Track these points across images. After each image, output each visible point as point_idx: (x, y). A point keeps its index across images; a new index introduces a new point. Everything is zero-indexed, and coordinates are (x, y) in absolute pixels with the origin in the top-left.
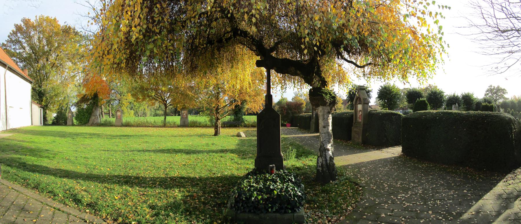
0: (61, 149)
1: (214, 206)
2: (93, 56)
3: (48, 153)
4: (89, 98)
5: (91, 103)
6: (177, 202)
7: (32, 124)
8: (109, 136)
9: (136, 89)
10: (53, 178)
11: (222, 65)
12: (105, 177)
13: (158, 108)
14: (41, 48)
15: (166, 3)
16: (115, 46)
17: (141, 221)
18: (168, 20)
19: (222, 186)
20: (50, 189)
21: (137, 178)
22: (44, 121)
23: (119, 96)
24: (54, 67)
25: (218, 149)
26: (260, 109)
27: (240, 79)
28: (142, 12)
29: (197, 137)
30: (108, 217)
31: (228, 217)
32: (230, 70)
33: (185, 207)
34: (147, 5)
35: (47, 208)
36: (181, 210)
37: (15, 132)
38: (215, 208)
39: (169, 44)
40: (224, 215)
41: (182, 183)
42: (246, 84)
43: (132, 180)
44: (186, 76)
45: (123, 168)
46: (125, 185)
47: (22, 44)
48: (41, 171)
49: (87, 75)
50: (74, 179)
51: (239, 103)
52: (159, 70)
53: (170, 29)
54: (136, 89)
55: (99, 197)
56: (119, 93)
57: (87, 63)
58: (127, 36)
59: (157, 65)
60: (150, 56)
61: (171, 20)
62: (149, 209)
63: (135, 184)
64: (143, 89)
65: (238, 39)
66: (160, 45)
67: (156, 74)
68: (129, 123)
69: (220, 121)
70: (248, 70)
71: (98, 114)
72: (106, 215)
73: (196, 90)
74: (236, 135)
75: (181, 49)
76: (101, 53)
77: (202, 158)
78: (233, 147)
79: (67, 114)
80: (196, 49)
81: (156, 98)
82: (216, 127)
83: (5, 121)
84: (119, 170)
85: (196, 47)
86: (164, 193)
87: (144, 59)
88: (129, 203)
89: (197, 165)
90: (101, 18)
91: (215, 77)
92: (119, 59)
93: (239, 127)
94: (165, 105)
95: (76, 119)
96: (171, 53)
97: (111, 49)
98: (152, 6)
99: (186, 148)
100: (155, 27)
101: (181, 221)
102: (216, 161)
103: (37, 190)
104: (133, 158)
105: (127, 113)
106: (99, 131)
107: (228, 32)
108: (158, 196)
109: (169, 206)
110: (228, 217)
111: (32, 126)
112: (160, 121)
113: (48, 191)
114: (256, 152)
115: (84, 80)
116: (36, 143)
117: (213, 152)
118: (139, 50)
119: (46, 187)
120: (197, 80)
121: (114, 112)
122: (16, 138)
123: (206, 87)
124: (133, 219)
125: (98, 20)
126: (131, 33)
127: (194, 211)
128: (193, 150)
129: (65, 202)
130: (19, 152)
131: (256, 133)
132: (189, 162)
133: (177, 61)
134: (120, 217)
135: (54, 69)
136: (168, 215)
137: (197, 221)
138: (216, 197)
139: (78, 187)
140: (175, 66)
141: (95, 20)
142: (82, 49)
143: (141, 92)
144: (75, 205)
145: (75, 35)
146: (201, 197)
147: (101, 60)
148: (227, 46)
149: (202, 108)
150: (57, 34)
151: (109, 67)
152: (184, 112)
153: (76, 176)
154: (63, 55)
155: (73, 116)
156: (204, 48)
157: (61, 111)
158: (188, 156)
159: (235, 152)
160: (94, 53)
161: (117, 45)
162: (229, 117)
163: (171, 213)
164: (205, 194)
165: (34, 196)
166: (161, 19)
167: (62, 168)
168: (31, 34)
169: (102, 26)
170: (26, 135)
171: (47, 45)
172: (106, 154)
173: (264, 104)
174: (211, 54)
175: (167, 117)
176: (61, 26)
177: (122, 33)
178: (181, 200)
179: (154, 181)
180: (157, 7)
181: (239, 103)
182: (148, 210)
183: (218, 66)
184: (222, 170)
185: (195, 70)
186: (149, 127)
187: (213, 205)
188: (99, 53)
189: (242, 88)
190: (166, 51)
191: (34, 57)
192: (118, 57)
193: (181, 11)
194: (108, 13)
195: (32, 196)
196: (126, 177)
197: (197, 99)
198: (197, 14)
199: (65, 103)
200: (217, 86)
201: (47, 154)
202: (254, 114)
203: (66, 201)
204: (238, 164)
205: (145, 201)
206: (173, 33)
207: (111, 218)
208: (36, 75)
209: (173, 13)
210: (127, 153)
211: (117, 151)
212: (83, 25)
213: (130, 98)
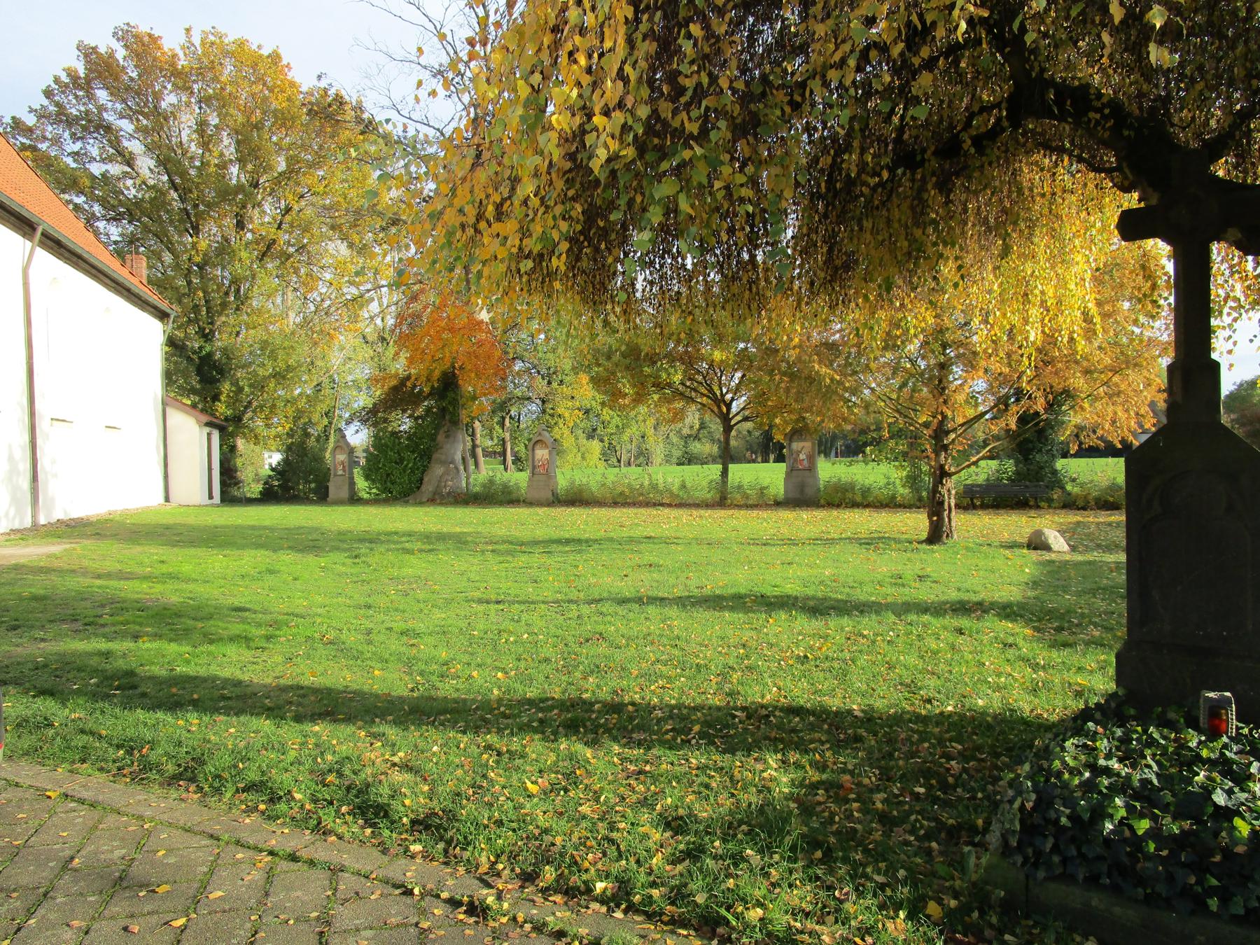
0: (300, 604)
1: (929, 836)
2: (439, 225)
3: (244, 621)
4: (421, 391)
5: (428, 410)
6: (775, 808)
7: (167, 499)
8: (504, 542)
9: (609, 358)
10: (265, 725)
11: (961, 249)
12: (486, 706)
13: (694, 432)
14: (212, 169)
15: (727, 18)
16: (527, 188)
17: (629, 880)
18: (735, 85)
19: (963, 757)
20: (253, 776)
21: (615, 708)
22: (223, 484)
23: (540, 384)
24: (273, 258)
25: (943, 598)
26: (1141, 426)
27: (1043, 302)
28: (630, 54)
29: (855, 548)
30: (500, 866)
31: (988, 888)
32: (996, 268)
33: (805, 829)
34: (652, 30)
35: (239, 856)
36: (788, 840)
37: (84, 536)
38: (934, 845)
39: (741, 179)
40: (974, 877)
41: (794, 731)
42: (1070, 321)
43: (594, 716)
44: (807, 304)
45: (557, 670)
46: (566, 736)
47: (119, 141)
48: (211, 699)
49: (414, 298)
50: (360, 723)
51: (1040, 406)
52: (698, 282)
53: (744, 120)
54: (609, 358)
55: (464, 787)
56: (544, 371)
57: (413, 250)
58: (574, 148)
59: (693, 264)
60: (664, 229)
61: (747, 84)
62: (660, 830)
63: (608, 731)
64: (638, 359)
65: (1032, 131)
66: (705, 181)
67: (689, 298)
68: (581, 491)
69: (950, 483)
70: (1079, 258)
71: (458, 457)
72: (492, 858)
73: (848, 358)
74: (1025, 540)
75: (788, 194)
76: (471, 212)
77: (876, 635)
78: (1011, 593)
79: (328, 455)
80: (849, 192)
81: (687, 394)
82: (936, 508)
83: (25, 484)
84: (541, 678)
85: (850, 183)
86: (722, 769)
87: (641, 238)
88: (585, 809)
89: (853, 661)
90: (468, 74)
91: (931, 302)
92: (544, 237)
93: (1038, 507)
94: (726, 419)
95: (367, 477)
96: (747, 213)
97: (510, 197)
98: (671, 33)
99: (810, 592)
100: (684, 113)
101: (790, 886)
102: (934, 646)
103: (192, 788)
104: (600, 628)
105: (575, 450)
106: (463, 524)
107: (986, 109)
108: (699, 780)
109: (741, 822)
110: (988, 888)
111: (169, 507)
112: (705, 483)
113: (241, 785)
114: (1124, 621)
115: (400, 317)
116: (188, 580)
117: (924, 608)
118: (622, 202)
119: (235, 766)
120: (855, 315)
121: (521, 448)
122: (86, 563)
123: (890, 344)
124: (598, 870)
125: (457, 80)
126: (590, 139)
127: (843, 849)
128: (838, 601)
129: (319, 823)
130: (103, 626)
131: (1120, 536)
132: (820, 649)
133: (772, 245)
134: (548, 863)
135: (270, 266)
136: (738, 859)
137: (857, 890)
138: (935, 800)
139: (375, 754)
140: (764, 263)
141: (445, 79)
142: (394, 193)
143: (627, 368)
144: (363, 827)
145: (362, 133)
146: (871, 791)
147: (472, 239)
148: (982, 166)
149: (873, 427)
150: (284, 120)
151: (502, 268)
152: (802, 448)
153: (367, 711)
154: (309, 212)
155: (353, 463)
156: (881, 184)
157: (304, 443)
158: (817, 624)
159: (1022, 616)
160: (441, 213)
161: (536, 182)
162: (994, 464)
163: (749, 851)
164: (888, 780)
165: (177, 814)
166: (705, 80)
167: (309, 680)
168: (164, 105)
169: (476, 107)
170: (139, 549)
171: (241, 161)
172: (493, 613)
173: (1162, 405)
174: (912, 208)
175: (731, 467)
176: (304, 89)
177: (554, 135)
178: (789, 797)
179: (683, 718)
180: (689, 36)
181: (1040, 406)
182: (658, 836)
183: (941, 256)
184: (961, 689)
185: (844, 276)
186: (662, 505)
187: (922, 832)
188: (461, 211)
189: (1050, 339)
190: (726, 207)
191: (177, 205)
192: (540, 230)
193: (787, 46)
194: (497, 57)
195: (165, 817)
196: (573, 706)
197: (855, 391)
198: (852, 52)
199: (322, 407)
200: (938, 338)
201: (241, 626)
202: (1109, 451)
203: (324, 818)
204: (1036, 667)
205: (645, 798)
206: (755, 135)
207: (513, 870)
208: (189, 283)
209: (752, 56)
210: (573, 611)
211: (533, 603)
212: (396, 97)
213: (587, 394)
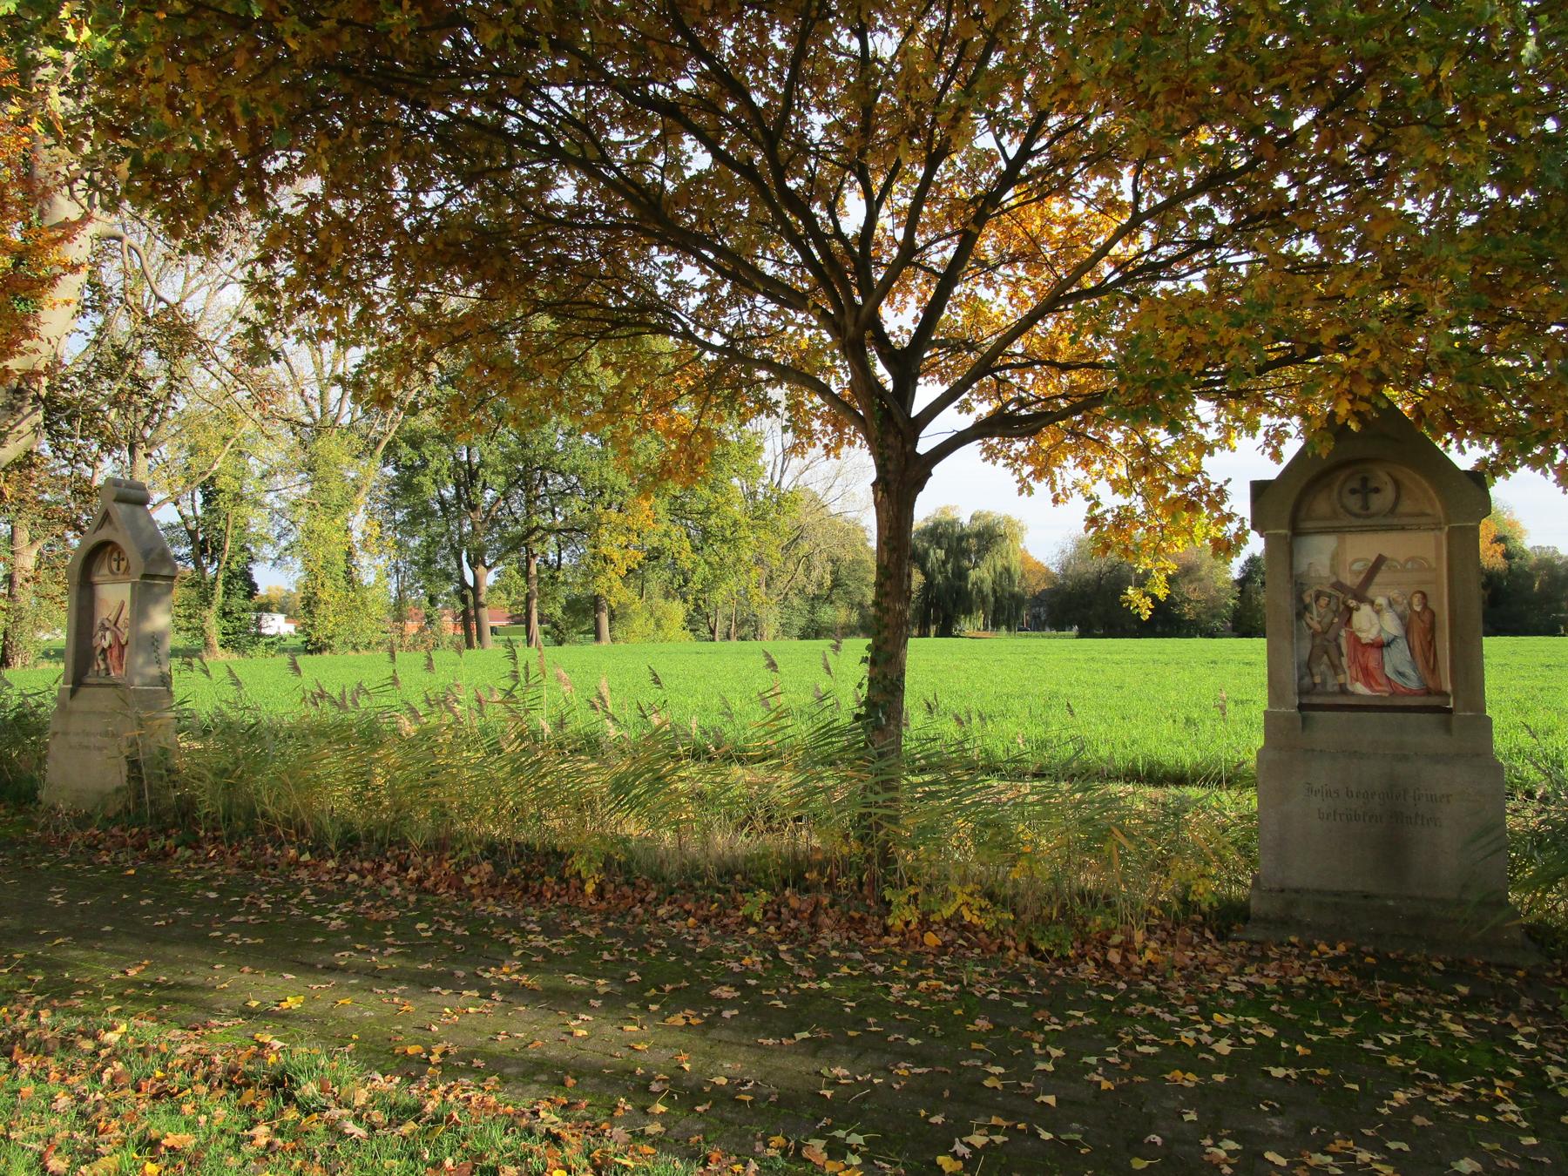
13: (824, 592)
